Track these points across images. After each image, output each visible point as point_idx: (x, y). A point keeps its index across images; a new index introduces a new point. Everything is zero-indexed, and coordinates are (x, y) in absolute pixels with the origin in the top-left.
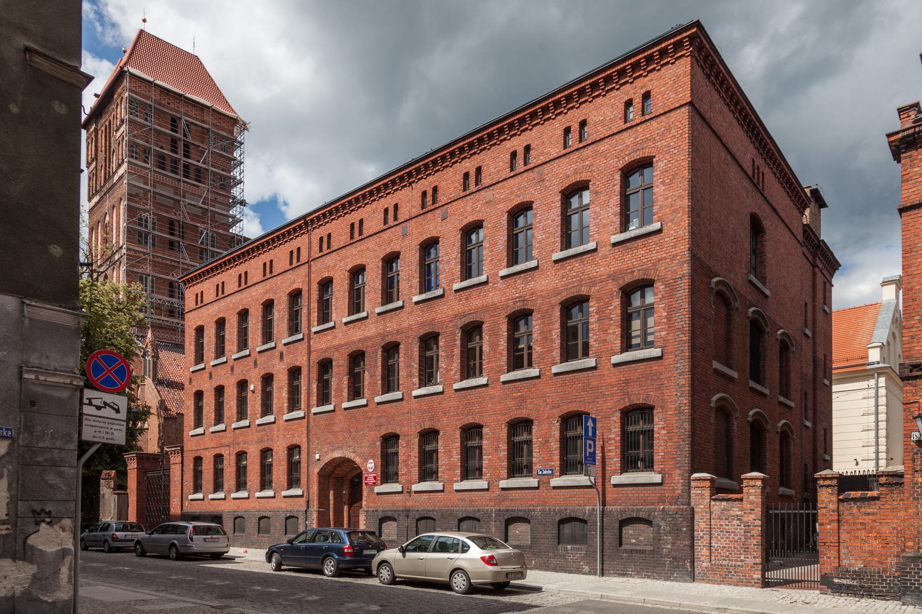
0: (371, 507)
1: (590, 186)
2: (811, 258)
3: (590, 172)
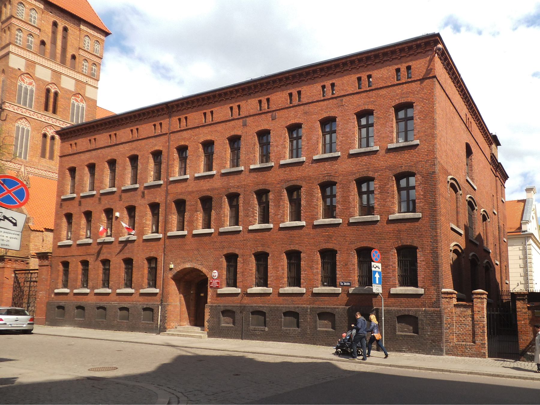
0: (214, 303)
1: (374, 113)
2: (494, 172)
3: (374, 105)
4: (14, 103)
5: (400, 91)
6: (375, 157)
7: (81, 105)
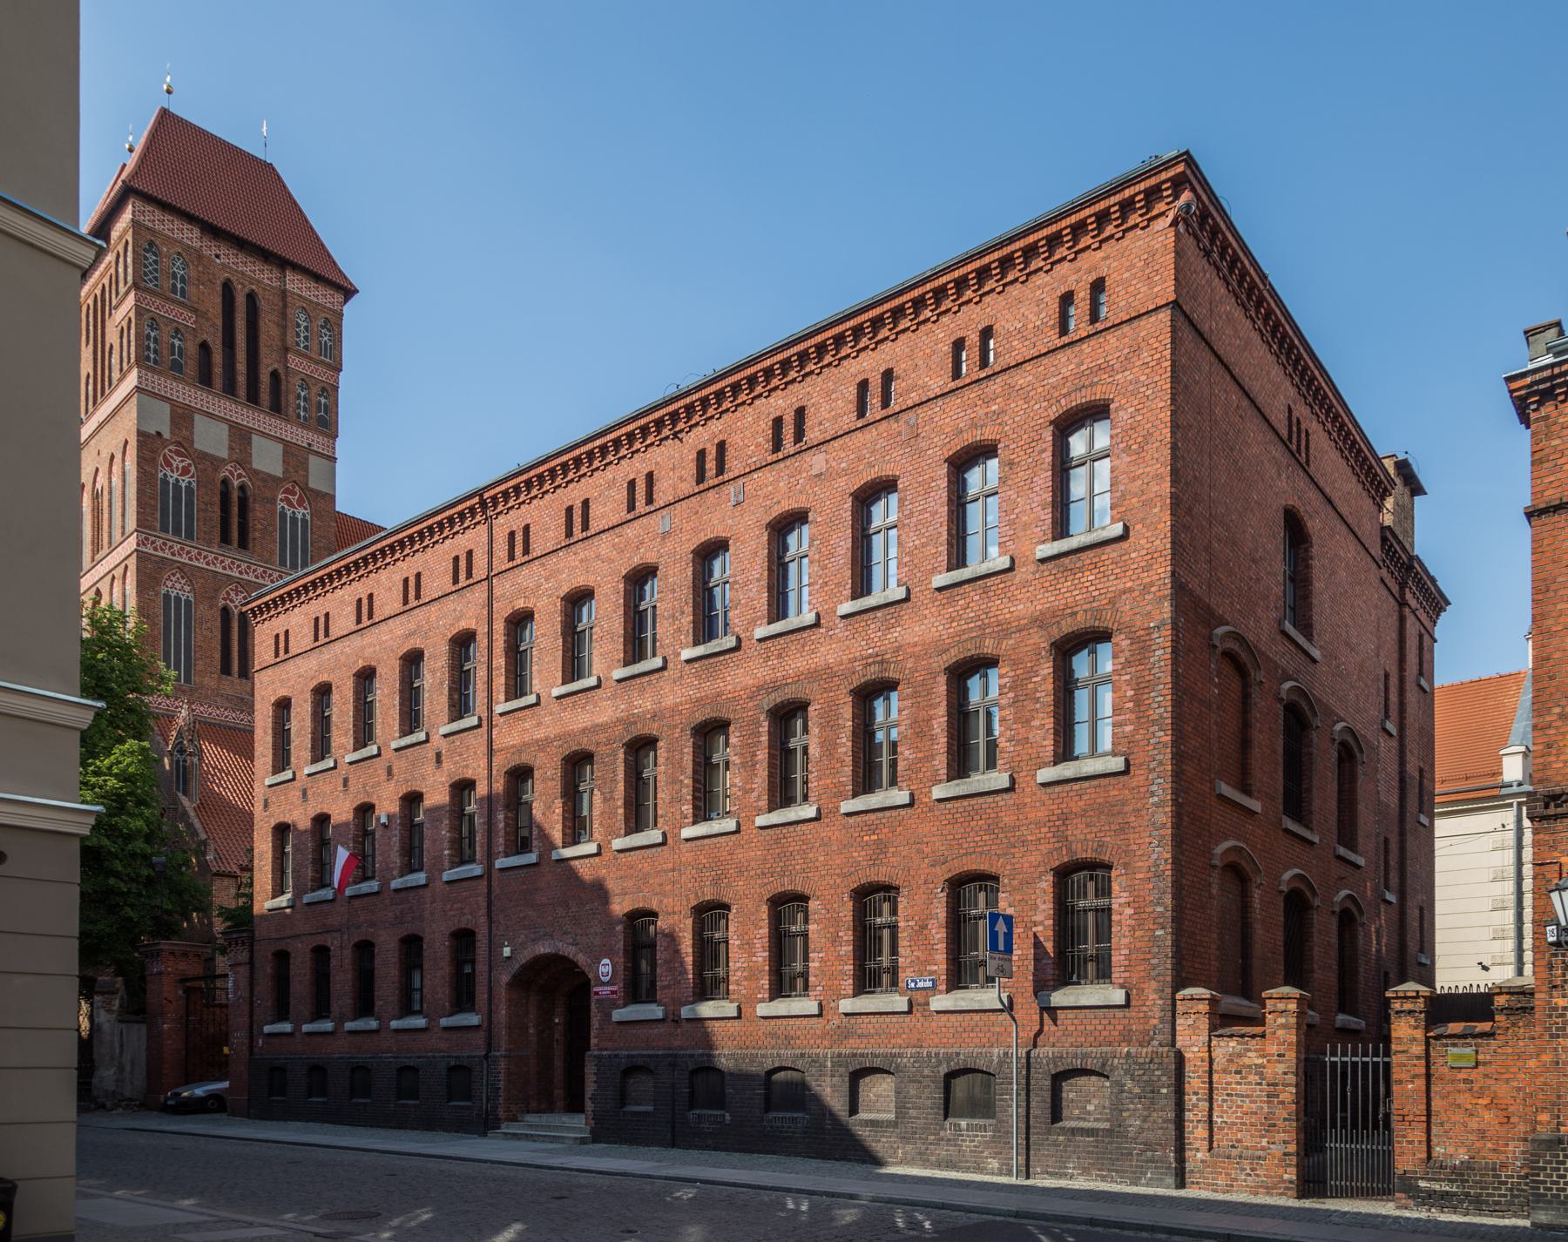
0: (606, 1049)
4: (155, 530)
5: (1072, 366)
6: (1000, 591)
7: (300, 512)
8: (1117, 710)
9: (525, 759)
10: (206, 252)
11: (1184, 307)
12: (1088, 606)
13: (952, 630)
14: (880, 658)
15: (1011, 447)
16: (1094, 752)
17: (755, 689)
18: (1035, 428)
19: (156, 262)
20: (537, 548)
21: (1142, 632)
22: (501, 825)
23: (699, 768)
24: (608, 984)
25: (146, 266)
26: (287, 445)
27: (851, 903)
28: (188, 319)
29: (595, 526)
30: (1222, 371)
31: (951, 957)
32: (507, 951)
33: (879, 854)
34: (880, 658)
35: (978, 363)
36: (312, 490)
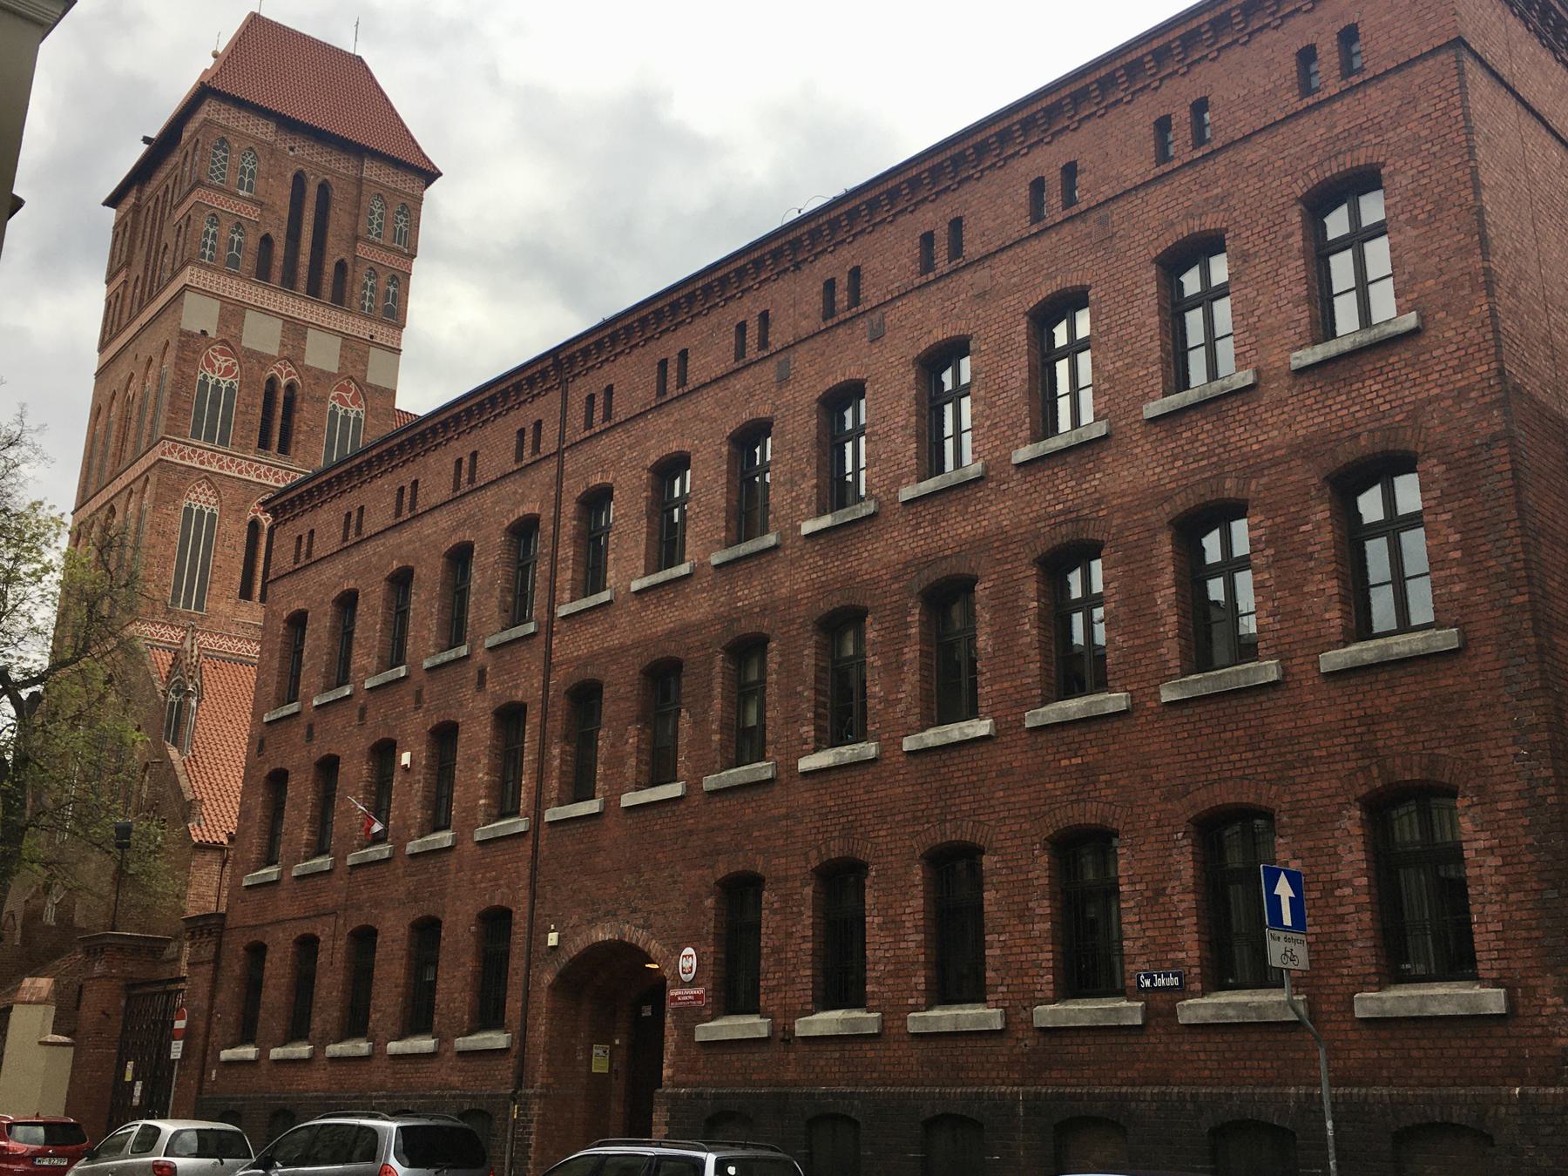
0: (1067, 1085)
8: (1435, 562)
9: (591, 673)
10: (280, 146)
11: (1472, 45)
12: (1377, 424)
13: (1175, 471)
14: (1074, 515)
15: (1243, 235)
16: (1404, 625)
17: (900, 566)
18: (1276, 209)
19: (225, 159)
20: (621, 412)
21: (1464, 453)
22: (557, 763)
23: (823, 675)
24: (691, 984)
25: (214, 163)
26: (346, 337)
27: (1046, 858)
28: (253, 213)
29: (694, 379)
30: (1533, 121)
31: (1207, 938)
32: (553, 939)
33: (1084, 785)
34: (1074, 515)
35: (1190, 142)
36: (370, 386)
